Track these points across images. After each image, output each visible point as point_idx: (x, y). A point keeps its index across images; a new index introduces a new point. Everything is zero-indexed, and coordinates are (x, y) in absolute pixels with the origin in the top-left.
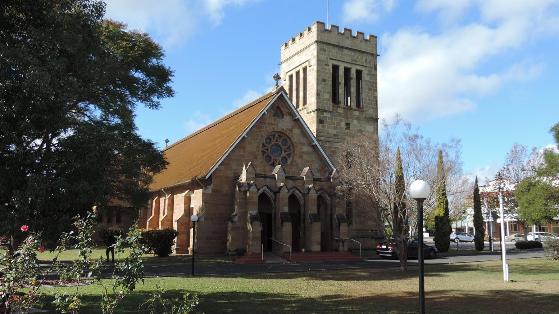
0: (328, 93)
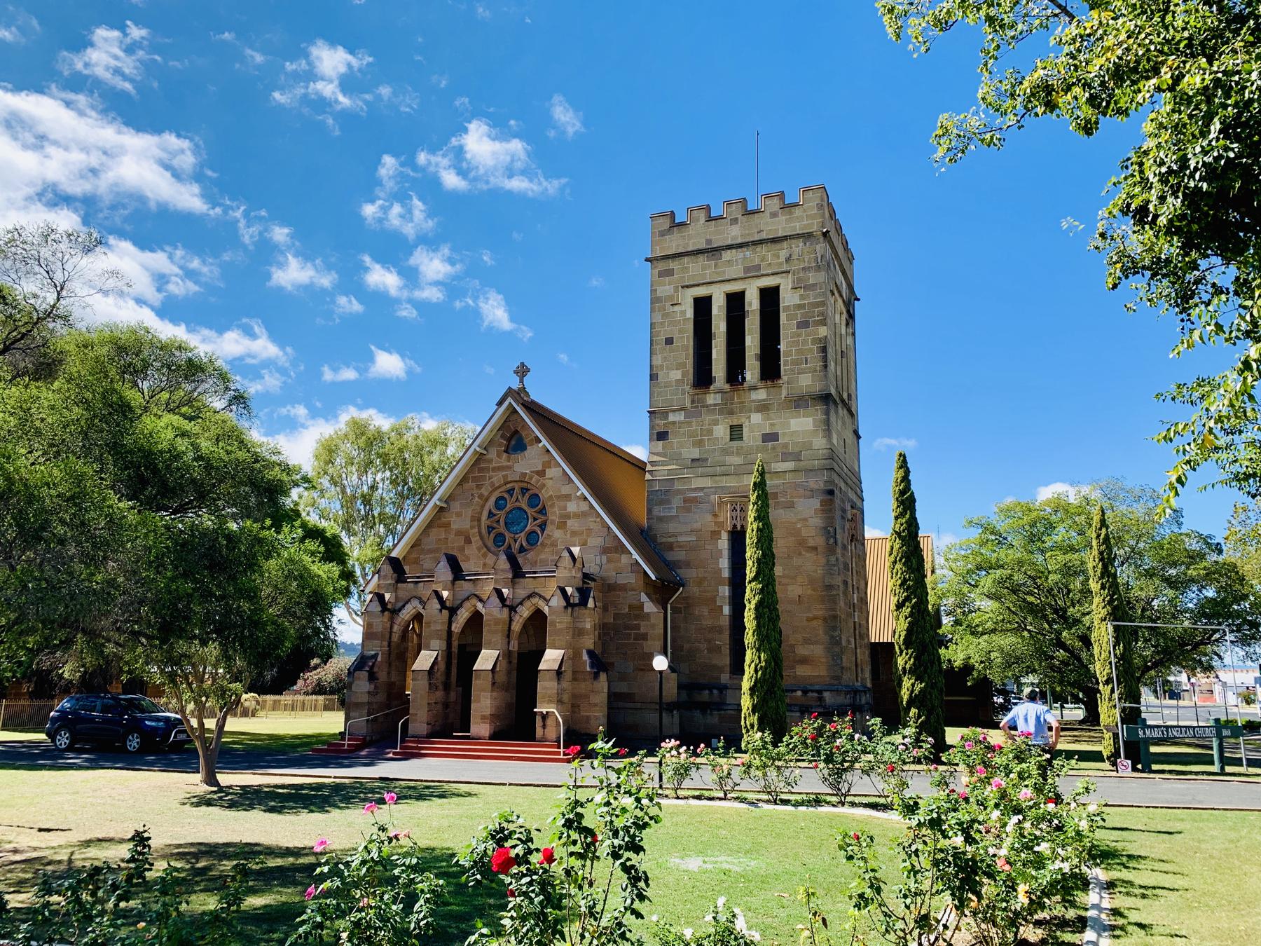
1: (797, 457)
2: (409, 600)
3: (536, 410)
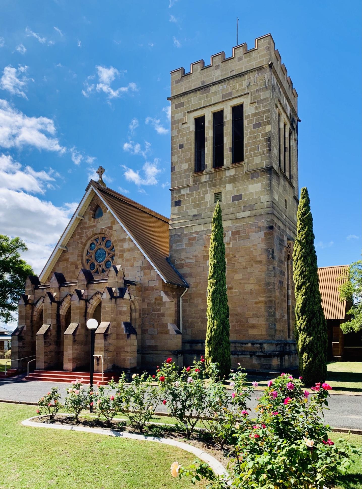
0: (187, 161)
1: (251, 208)
2: (40, 298)
3: (107, 193)
